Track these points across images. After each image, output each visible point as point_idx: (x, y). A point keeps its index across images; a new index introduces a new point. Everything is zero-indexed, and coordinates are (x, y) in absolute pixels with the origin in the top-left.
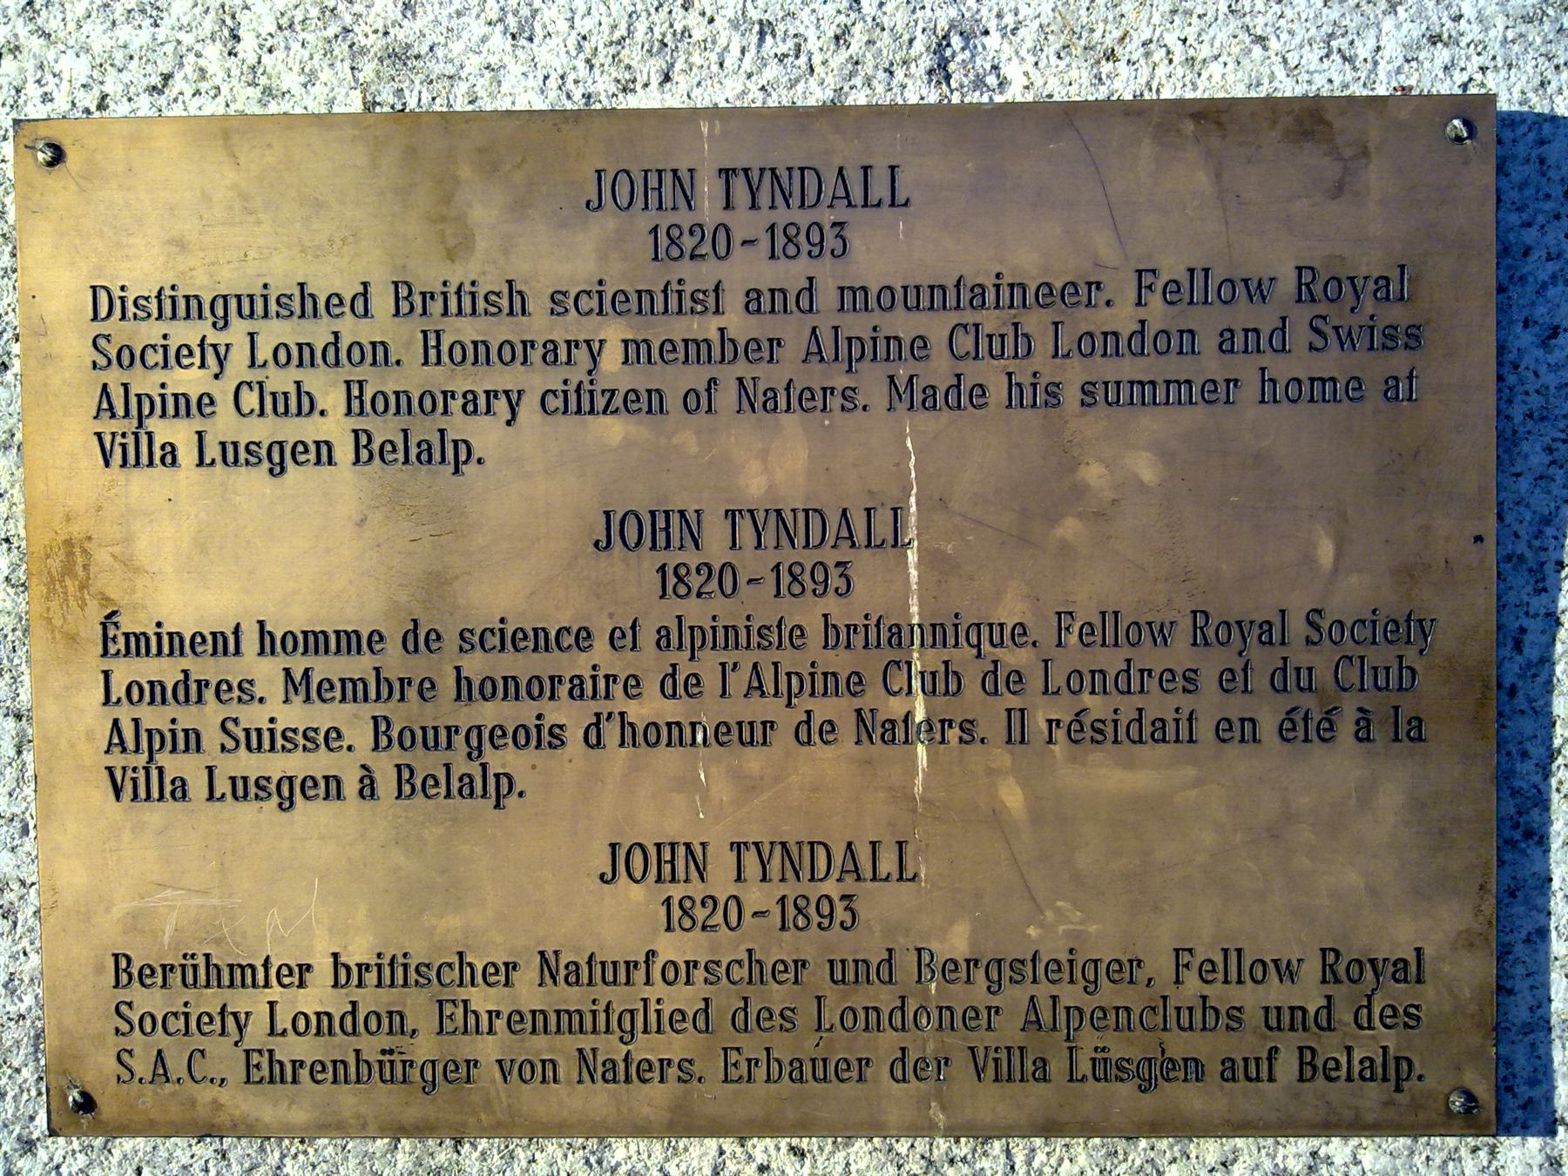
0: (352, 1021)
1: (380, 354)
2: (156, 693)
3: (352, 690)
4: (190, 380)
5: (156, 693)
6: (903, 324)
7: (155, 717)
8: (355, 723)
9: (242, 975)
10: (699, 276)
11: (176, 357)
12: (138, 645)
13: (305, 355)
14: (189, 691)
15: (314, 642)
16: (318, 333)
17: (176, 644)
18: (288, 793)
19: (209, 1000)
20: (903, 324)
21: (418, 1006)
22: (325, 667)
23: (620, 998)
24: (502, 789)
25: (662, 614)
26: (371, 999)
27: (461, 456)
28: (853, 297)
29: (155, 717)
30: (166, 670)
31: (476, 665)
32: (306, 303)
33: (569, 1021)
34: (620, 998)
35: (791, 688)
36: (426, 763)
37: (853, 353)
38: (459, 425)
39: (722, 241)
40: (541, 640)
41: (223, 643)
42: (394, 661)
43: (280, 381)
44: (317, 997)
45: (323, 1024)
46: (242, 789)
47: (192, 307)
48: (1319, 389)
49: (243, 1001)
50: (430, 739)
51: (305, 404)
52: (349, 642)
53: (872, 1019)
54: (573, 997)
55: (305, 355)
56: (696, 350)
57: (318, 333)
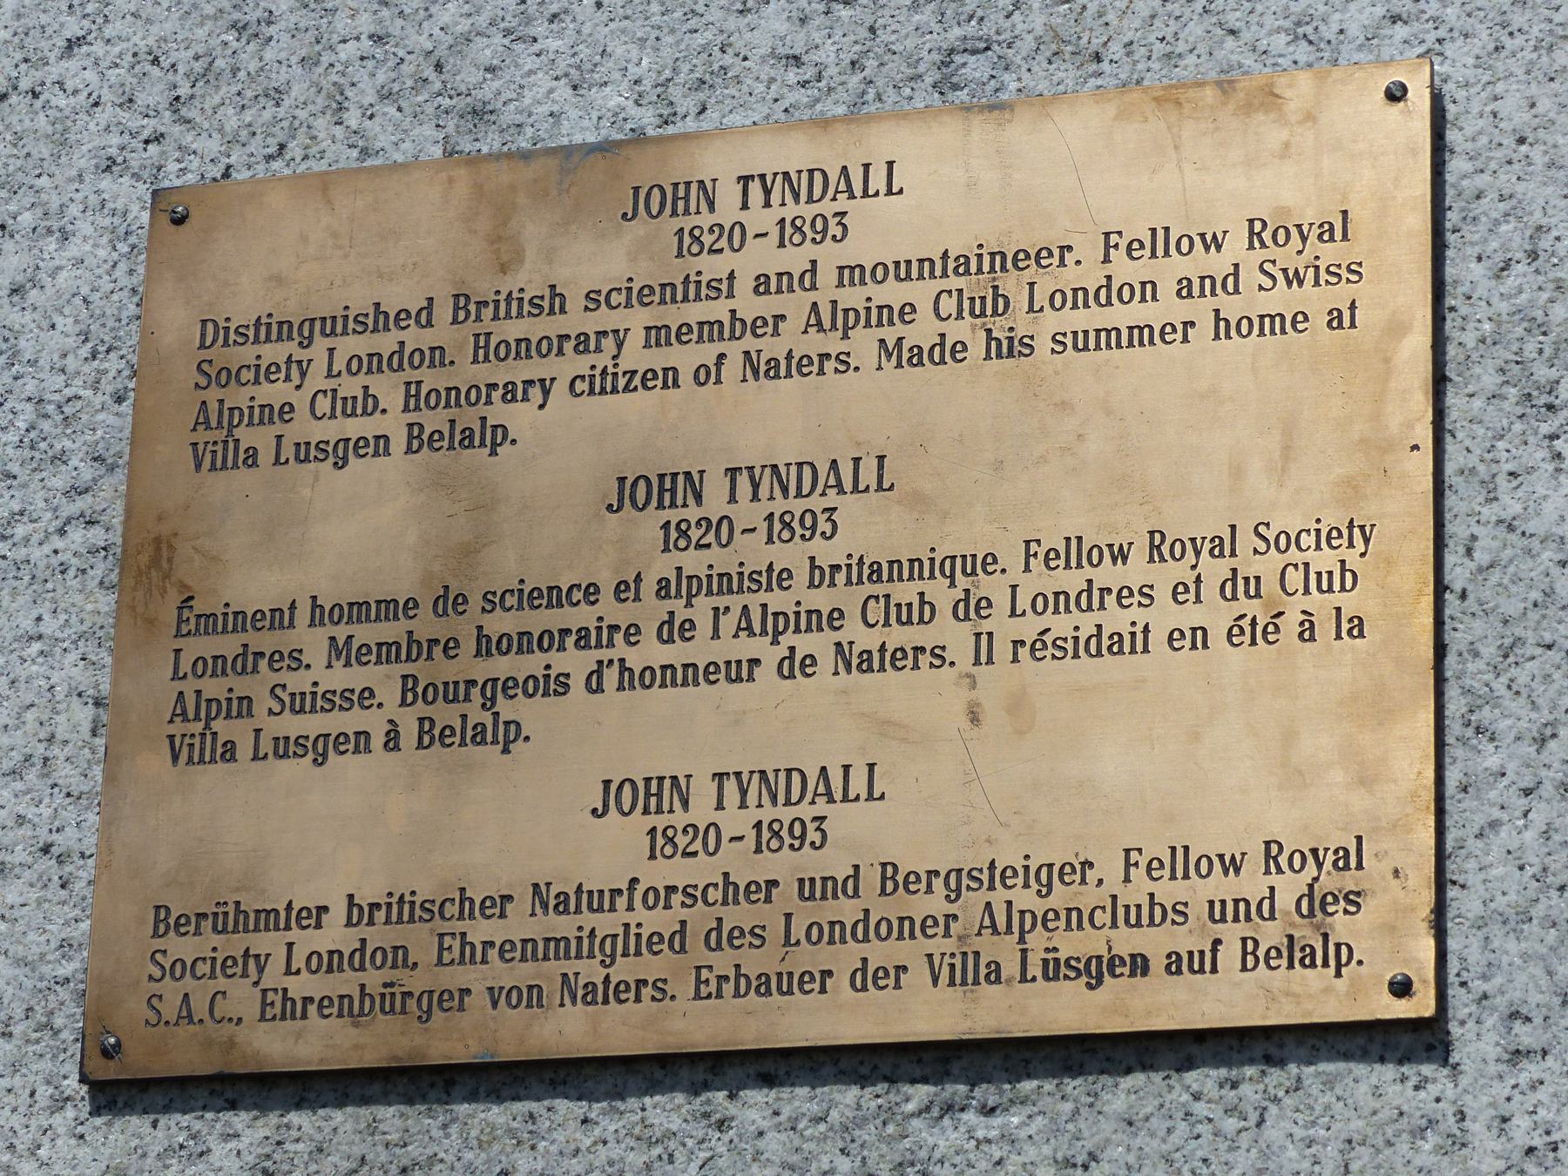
0: (360, 957)
1: (437, 356)
2: (218, 666)
3: (387, 652)
4: (274, 393)
5: (218, 666)
6: (892, 293)
7: (213, 687)
8: (384, 680)
9: (267, 919)
10: (713, 267)
11: (267, 373)
12: (208, 624)
13: (374, 363)
14: (247, 661)
15: (358, 610)
16: (386, 343)
17: (240, 620)
18: (321, 749)
19: (234, 944)
20: (892, 293)
21: (419, 939)
22: (367, 633)
23: (606, 924)
24: (510, 736)
25: (662, 566)
26: (379, 935)
27: (497, 438)
28: (850, 274)
29: (213, 687)
30: (229, 645)
31: (500, 623)
32: (380, 320)
33: (557, 946)
34: (606, 924)
35: (775, 625)
36: (445, 714)
37: (846, 321)
38: (498, 412)
39: (735, 237)
40: (555, 597)
41: (280, 618)
42: (426, 625)
43: (350, 387)
44: (335, 935)
45: (332, 962)
46: (284, 748)
47: (285, 330)
48: (1272, 323)
49: (268, 943)
50: (453, 693)
51: (370, 405)
52: (389, 608)
53: (835, 933)
54: (564, 925)
55: (374, 363)
56: (710, 330)
57: (386, 343)
